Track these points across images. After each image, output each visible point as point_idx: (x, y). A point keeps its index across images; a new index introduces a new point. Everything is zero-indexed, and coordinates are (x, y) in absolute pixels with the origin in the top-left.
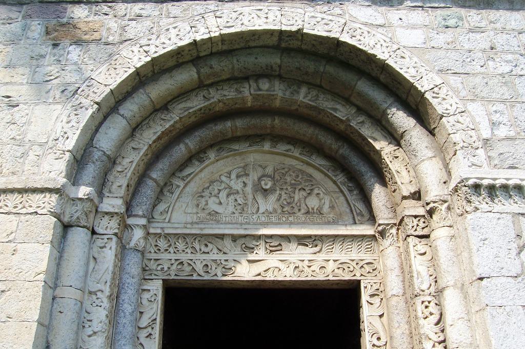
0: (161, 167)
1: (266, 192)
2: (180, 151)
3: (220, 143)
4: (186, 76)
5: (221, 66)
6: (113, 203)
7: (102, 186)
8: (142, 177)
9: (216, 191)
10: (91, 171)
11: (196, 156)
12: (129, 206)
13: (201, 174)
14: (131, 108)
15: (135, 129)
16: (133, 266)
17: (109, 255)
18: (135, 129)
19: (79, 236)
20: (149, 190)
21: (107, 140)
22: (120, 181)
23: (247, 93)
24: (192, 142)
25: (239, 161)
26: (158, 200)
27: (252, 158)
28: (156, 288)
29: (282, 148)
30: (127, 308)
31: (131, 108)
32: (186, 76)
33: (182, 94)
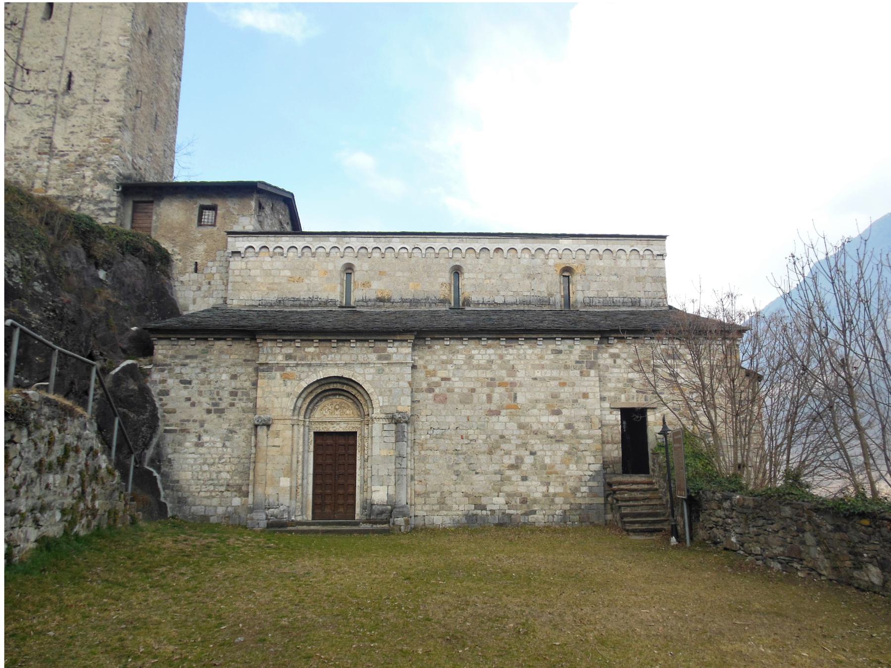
0: (573, 467)
1: (337, 409)
2: (316, 401)
3: (326, 397)
4: (317, 385)
5: (323, 382)
6: (301, 418)
7: (299, 415)
8: (307, 408)
9: (221, 371)
10: (296, 412)
11: (321, 400)
12: (305, 418)
13: (322, 404)
14: (303, 396)
15: (305, 399)
16: (307, 429)
17: (302, 429)
18: (305, 399)
19: (296, 427)
20: (309, 411)
21: (299, 404)
22: (303, 412)
23: (331, 387)
24: (318, 398)
25: (331, 401)
26: (311, 412)
27: (334, 400)
28: (312, 434)
29: (341, 397)
30: (306, 439)
31: (303, 396)
32: (317, 385)
33: (316, 388)
